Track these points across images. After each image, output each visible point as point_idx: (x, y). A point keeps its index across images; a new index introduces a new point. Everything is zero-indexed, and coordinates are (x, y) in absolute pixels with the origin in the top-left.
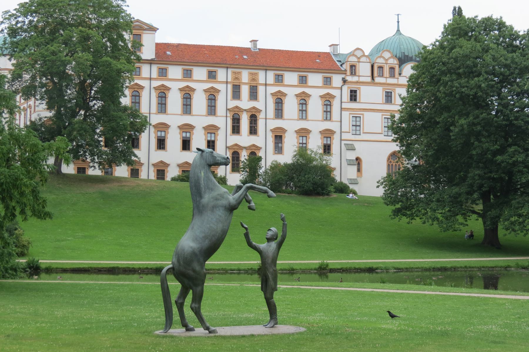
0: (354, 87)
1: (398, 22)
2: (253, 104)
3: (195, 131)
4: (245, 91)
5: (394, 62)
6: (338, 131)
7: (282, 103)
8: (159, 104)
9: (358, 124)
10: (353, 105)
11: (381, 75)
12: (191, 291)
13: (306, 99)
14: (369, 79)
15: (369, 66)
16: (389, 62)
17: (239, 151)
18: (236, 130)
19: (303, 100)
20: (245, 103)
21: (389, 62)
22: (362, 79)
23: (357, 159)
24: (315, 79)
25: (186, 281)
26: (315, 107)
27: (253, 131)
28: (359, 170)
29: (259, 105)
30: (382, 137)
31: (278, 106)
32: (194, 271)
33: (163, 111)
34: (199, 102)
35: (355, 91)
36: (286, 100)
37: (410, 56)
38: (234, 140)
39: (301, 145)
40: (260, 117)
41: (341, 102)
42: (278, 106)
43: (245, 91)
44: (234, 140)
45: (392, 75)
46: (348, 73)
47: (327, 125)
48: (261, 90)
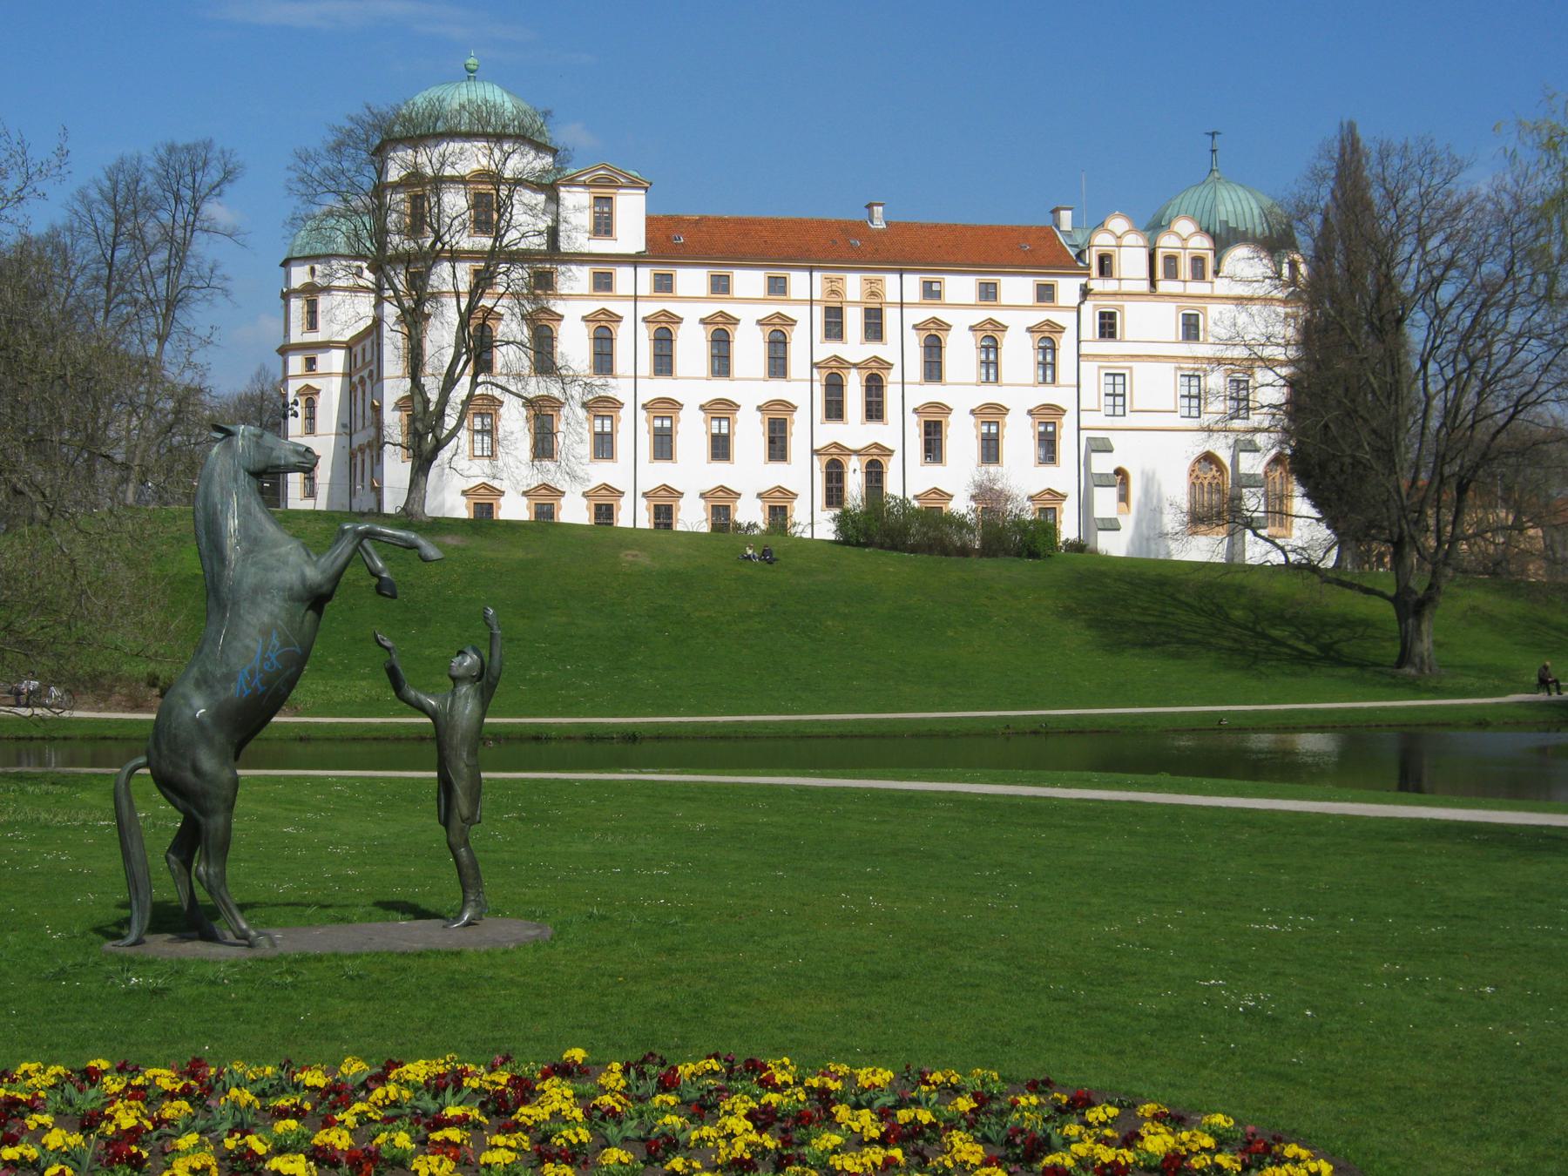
0: (1108, 305)
2: (874, 349)
3: (1008, 419)
4: (854, 320)
5: (1202, 244)
9: (1119, 390)
10: (1108, 347)
11: (1172, 273)
14: (1144, 286)
15: (1143, 255)
17: (843, 459)
18: (835, 410)
19: (990, 341)
20: (854, 347)
22: (1127, 286)
24: (1017, 288)
26: (1018, 352)
27: (874, 411)
29: (886, 350)
30: (1175, 421)
32: (197, 771)
34: (749, 347)
35: (1112, 315)
38: (829, 433)
40: (890, 379)
41: (1079, 342)
43: (854, 320)
44: (829, 433)
46: (1095, 271)
48: (891, 317)
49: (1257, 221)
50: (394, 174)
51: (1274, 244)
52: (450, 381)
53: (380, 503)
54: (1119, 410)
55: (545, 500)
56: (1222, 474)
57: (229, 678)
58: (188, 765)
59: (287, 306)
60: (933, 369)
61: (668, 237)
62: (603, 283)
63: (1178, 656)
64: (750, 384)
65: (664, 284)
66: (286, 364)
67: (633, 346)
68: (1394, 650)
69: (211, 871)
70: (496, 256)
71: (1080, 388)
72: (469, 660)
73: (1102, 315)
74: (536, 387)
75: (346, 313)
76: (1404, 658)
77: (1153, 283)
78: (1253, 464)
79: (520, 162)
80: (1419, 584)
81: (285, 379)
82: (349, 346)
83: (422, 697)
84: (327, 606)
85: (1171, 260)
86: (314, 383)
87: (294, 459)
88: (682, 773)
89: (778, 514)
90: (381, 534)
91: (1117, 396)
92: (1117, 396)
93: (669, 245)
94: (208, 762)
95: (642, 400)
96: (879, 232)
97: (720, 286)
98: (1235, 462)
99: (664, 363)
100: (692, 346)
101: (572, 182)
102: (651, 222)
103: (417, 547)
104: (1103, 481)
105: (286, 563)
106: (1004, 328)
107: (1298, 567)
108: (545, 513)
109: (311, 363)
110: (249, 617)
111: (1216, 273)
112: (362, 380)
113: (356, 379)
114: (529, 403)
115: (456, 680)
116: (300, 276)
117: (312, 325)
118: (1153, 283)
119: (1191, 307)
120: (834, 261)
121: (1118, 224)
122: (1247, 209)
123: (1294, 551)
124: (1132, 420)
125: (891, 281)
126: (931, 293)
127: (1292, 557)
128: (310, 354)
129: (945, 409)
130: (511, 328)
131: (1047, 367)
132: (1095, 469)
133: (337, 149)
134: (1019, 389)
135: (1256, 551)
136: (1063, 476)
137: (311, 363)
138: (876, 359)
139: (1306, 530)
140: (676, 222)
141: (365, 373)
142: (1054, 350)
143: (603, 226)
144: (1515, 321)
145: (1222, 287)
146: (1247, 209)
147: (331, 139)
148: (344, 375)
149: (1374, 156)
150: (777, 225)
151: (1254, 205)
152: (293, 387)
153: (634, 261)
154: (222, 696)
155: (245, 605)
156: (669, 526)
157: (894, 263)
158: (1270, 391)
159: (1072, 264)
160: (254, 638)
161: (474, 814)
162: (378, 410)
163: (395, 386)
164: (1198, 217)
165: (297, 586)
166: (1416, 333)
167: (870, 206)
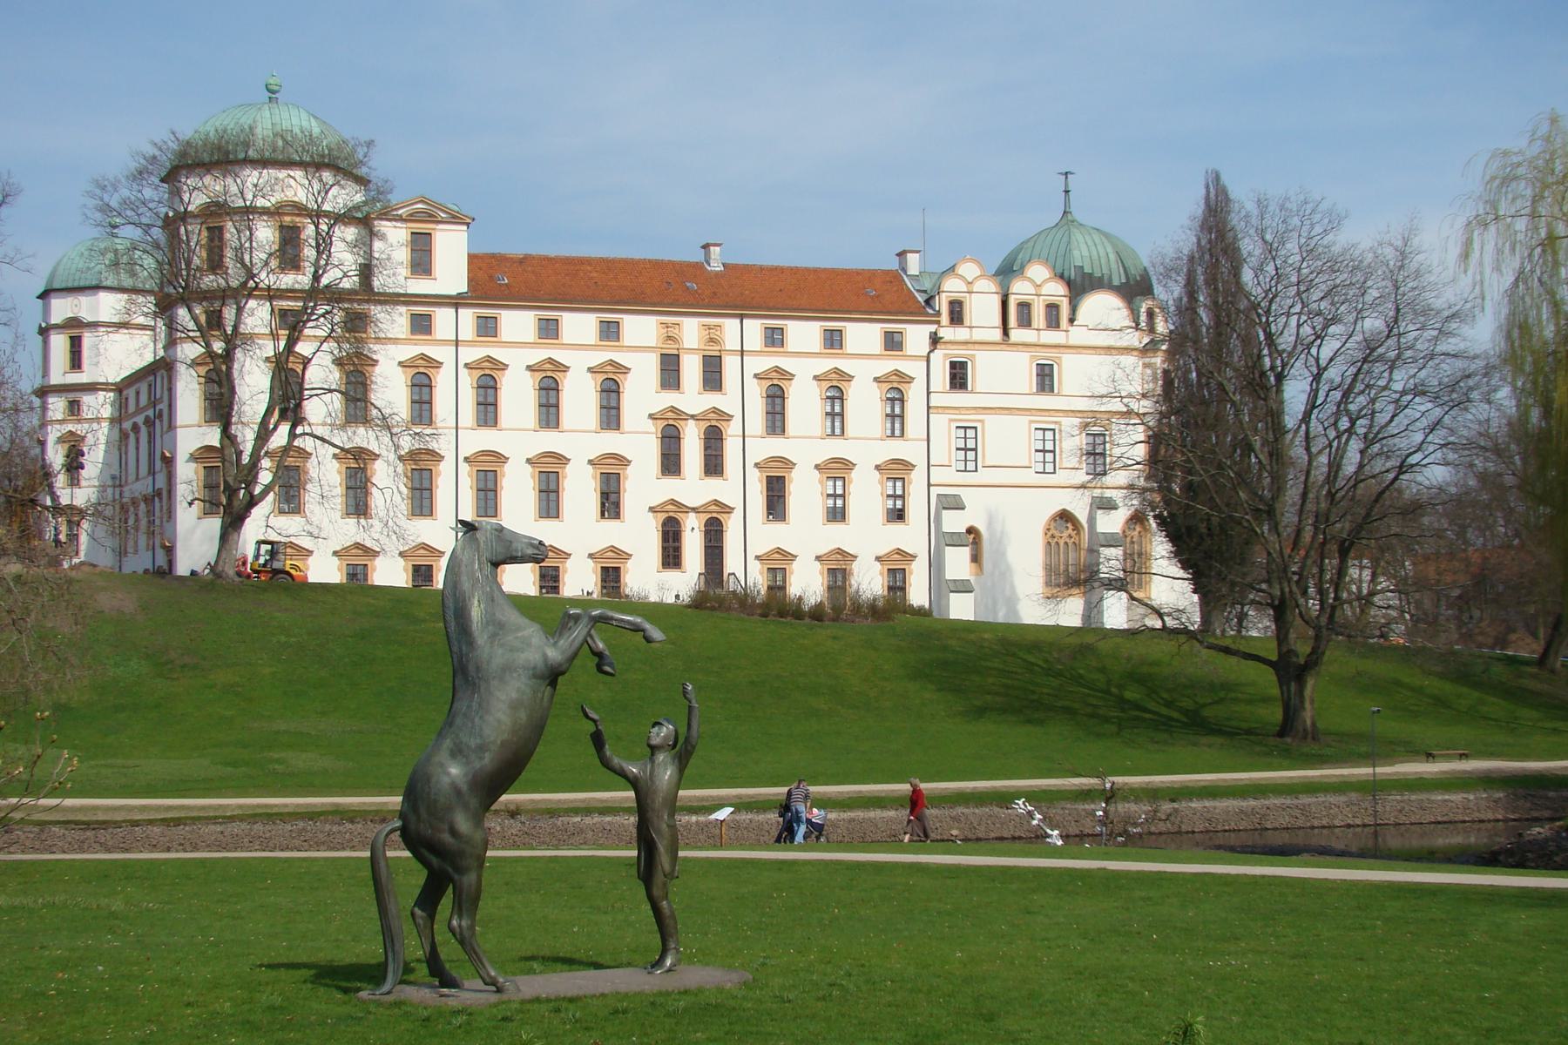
0: (959, 354)
1: (1067, 192)
2: (713, 400)
3: (854, 474)
4: (691, 369)
5: (1057, 290)
6: (919, 461)
7: (783, 398)
8: (479, 404)
9: (971, 444)
10: (959, 399)
11: (1026, 322)
12: (450, 890)
13: (558, 376)
14: (997, 335)
15: (996, 301)
16: (1044, 291)
17: (679, 516)
18: (671, 463)
19: (835, 392)
20: (692, 397)
21: (1044, 291)
22: (978, 335)
23: (971, 530)
24: (863, 335)
25: (434, 860)
26: (865, 403)
27: (713, 466)
28: (976, 558)
29: (726, 401)
30: (1029, 477)
31: (774, 404)
32: (453, 832)
33: (553, 424)
34: (580, 397)
35: (963, 365)
36: (566, 382)
37: (1097, 274)
38: (671, 489)
39: (830, 502)
40: (730, 432)
41: (929, 393)
42: (774, 404)
43: (691, 369)
44: (671, 489)
45: (1053, 321)
46: (945, 319)
47: (897, 449)
48: (730, 365)
49: (1114, 266)
50: (196, 201)
51: (1134, 289)
52: (264, 434)
53: (171, 563)
54: (971, 466)
55: (358, 558)
56: (1078, 534)
57: (482, 748)
58: (446, 827)
59: (46, 343)
60: (776, 421)
61: (491, 277)
62: (422, 325)
63: (1041, 722)
64: (580, 437)
65: (487, 328)
66: (44, 408)
67: (453, 395)
68: (1275, 714)
69: (464, 923)
70: (315, 293)
71: (931, 440)
72: (666, 730)
73: (953, 365)
74: (363, 437)
75: (120, 354)
76: (1287, 727)
77: (1006, 332)
78: (1111, 523)
79: (343, 196)
80: (1303, 649)
81: (44, 424)
82: (119, 388)
83: (624, 765)
84: (560, 679)
85: (1025, 307)
86: (79, 429)
87: (530, 551)
88: (1547, 769)
89: (611, 577)
90: (612, 618)
91: (969, 452)
92: (969, 452)
93: (494, 283)
94: (463, 823)
95: (466, 451)
96: (717, 273)
97: (549, 330)
98: (1092, 520)
99: (488, 411)
100: (519, 394)
101: (386, 215)
102: (473, 259)
103: (643, 630)
104: (954, 540)
105: (529, 645)
106: (850, 378)
107: (1174, 631)
108: (357, 575)
109: (74, 407)
110: (498, 694)
111: (1072, 321)
112: (135, 428)
113: (127, 425)
114: (345, 453)
115: (654, 749)
116: (61, 308)
117: (76, 363)
118: (1006, 332)
119: (1045, 357)
120: (671, 305)
121: (969, 270)
122: (1102, 253)
123: (1169, 615)
124: (984, 476)
125: (730, 326)
126: (774, 338)
127: (1170, 622)
128: (72, 396)
129: (788, 464)
130: (322, 372)
131: (896, 418)
132: (946, 529)
133: (140, 175)
134: (866, 443)
135: (1116, 613)
136: (912, 536)
137: (74, 407)
138: (715, 410)
139: (1171, 589)
140: (497, 260)
141: (140, 419)
142: (902, 401)
143: (422, 263)
144: (1400, 379)
145: (1077, 335)
146: (1102, 253)
147: (133, 165)
148: (112, 421)
149: (1250, 206)
150: (607, 265)
151: (1110, 249)
152: (53, 434)
153: (456, 302)
154: (477, 765)
155: (495, 683)
156: (556, 589)
157: (736, 307)
158: (1131, 444)
159: (920, 307)
160: (501, 711)
161: (673, 870)
162: (169, 462)
163: (192, 431)
164: (1052, 259)
165: (540, 665)
166: (1295, 394)
167: (706, 247)
